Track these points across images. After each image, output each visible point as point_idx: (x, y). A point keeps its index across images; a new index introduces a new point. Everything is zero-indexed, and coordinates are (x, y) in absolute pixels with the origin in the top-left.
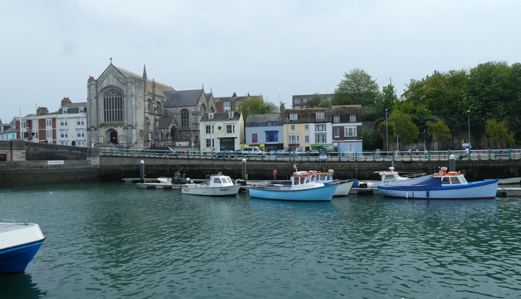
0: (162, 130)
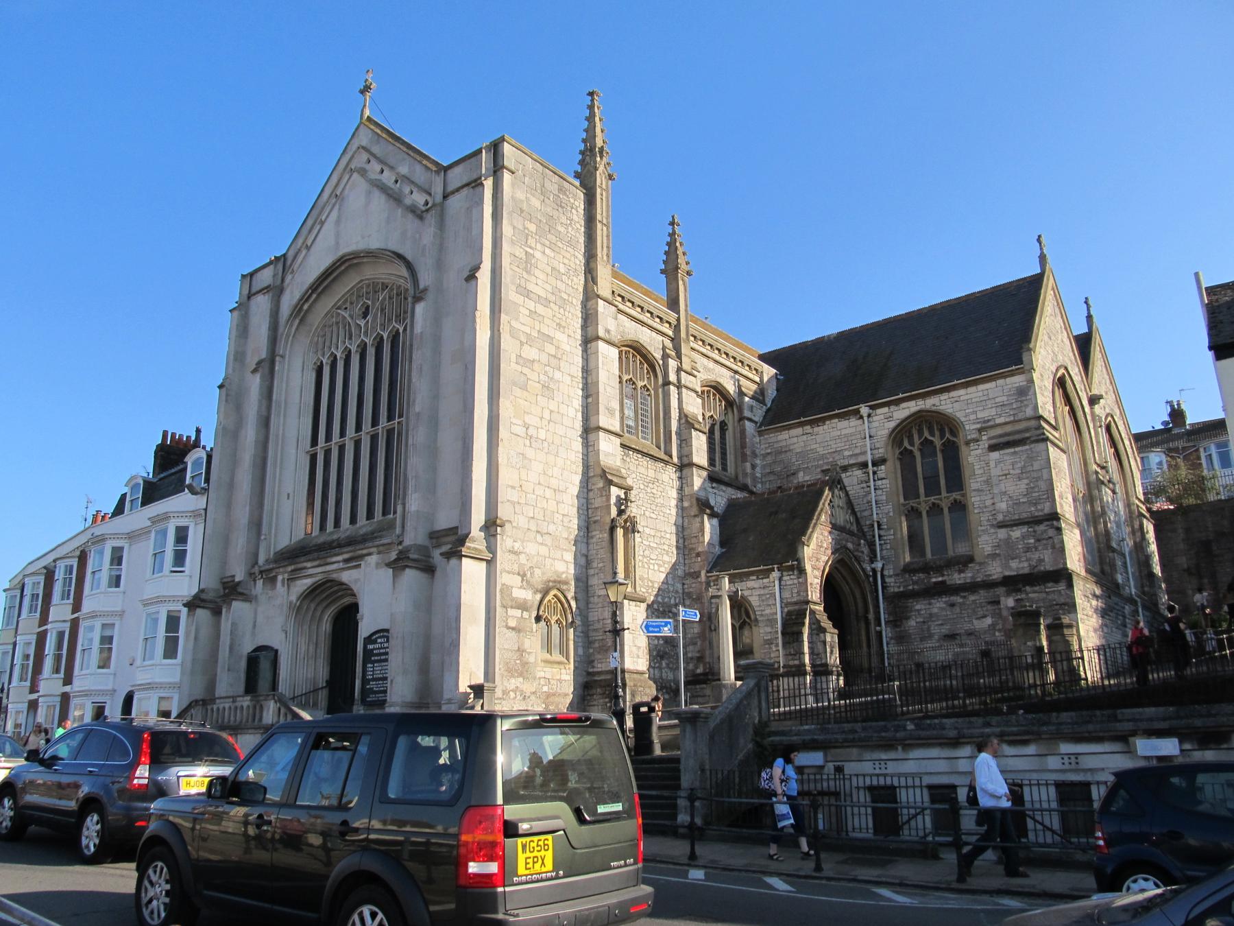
0: (752, 589)
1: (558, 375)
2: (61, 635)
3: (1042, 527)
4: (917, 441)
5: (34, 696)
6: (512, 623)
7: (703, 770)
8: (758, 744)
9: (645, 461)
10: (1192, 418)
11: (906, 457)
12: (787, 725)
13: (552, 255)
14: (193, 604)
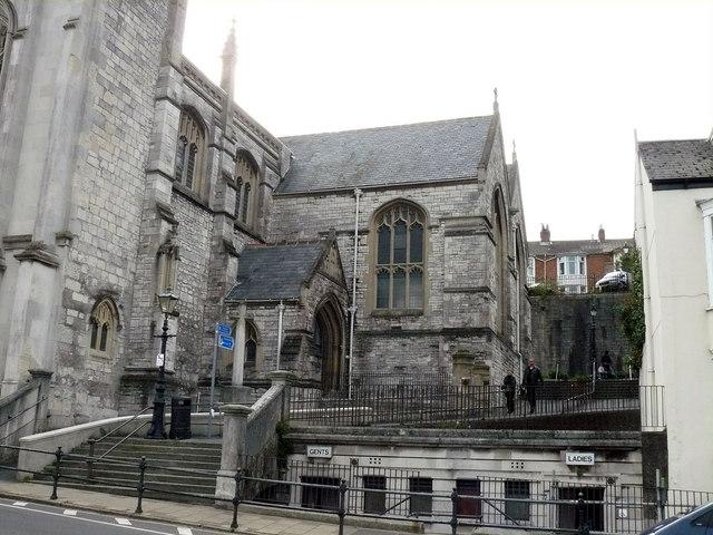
0: (262, 317)
1: (130, 122)
3: (475, 296)
4: (393, 221)
6: (70, 322)
7: (240, 455)
8: (280, 439)
9: (187, 204)
10: (554, 237)
11: (383, 231)
12: (302, 425)
13: (139, 22)
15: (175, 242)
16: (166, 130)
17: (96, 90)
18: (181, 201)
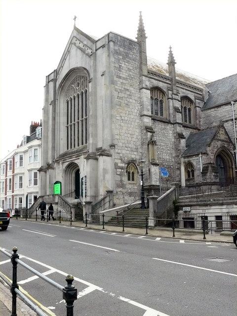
0: (194, 160)
1: (131, 100)
2: (10, 179)
5: (6, 196)
8: (175, 206)
9: (160, 123)
14: (40, 170)
15: (155, 139)
16: (145, 99)
17: (115, 94)
18: (157, 123)
